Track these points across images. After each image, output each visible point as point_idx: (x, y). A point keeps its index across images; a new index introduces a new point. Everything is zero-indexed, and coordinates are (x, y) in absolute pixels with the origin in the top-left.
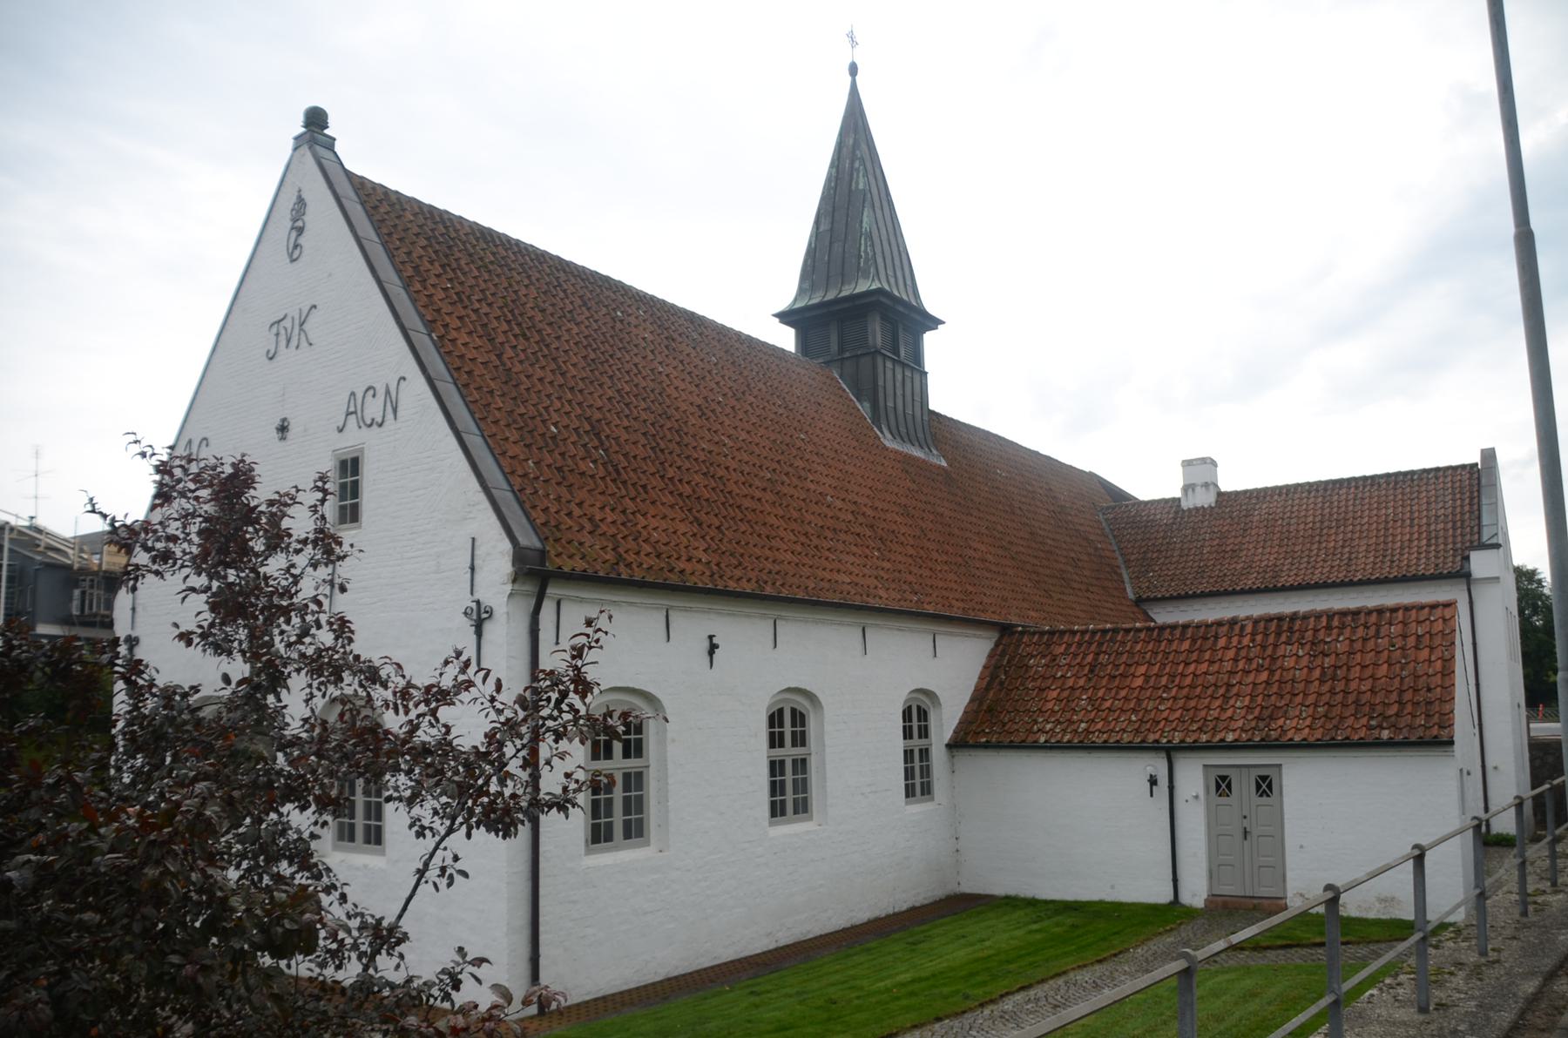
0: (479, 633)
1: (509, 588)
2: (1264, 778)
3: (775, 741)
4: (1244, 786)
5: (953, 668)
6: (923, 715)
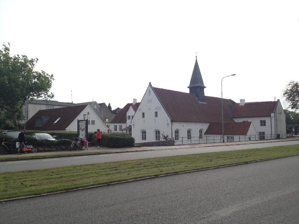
3: (188, 133)
5: (205, 127)
6: (202, 131)
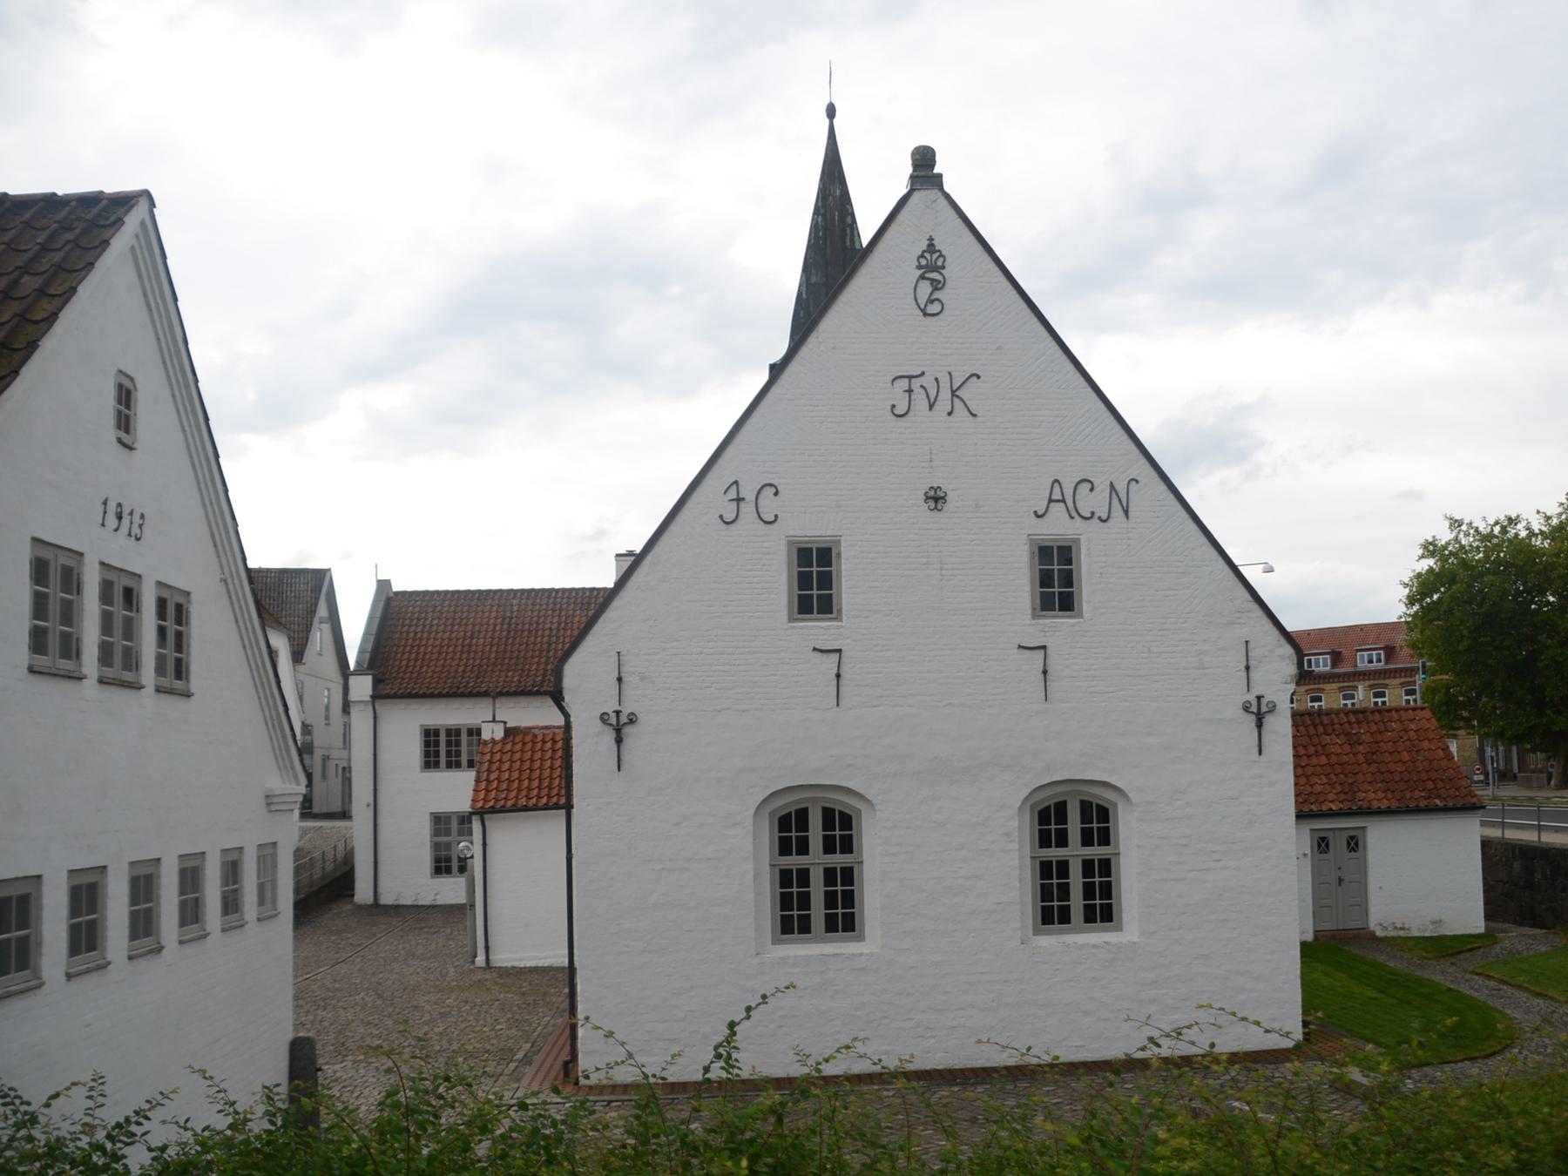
0: (1259, 725)
1: (1292, 687)
2: (1352, 838)
4: (1338, 844)
